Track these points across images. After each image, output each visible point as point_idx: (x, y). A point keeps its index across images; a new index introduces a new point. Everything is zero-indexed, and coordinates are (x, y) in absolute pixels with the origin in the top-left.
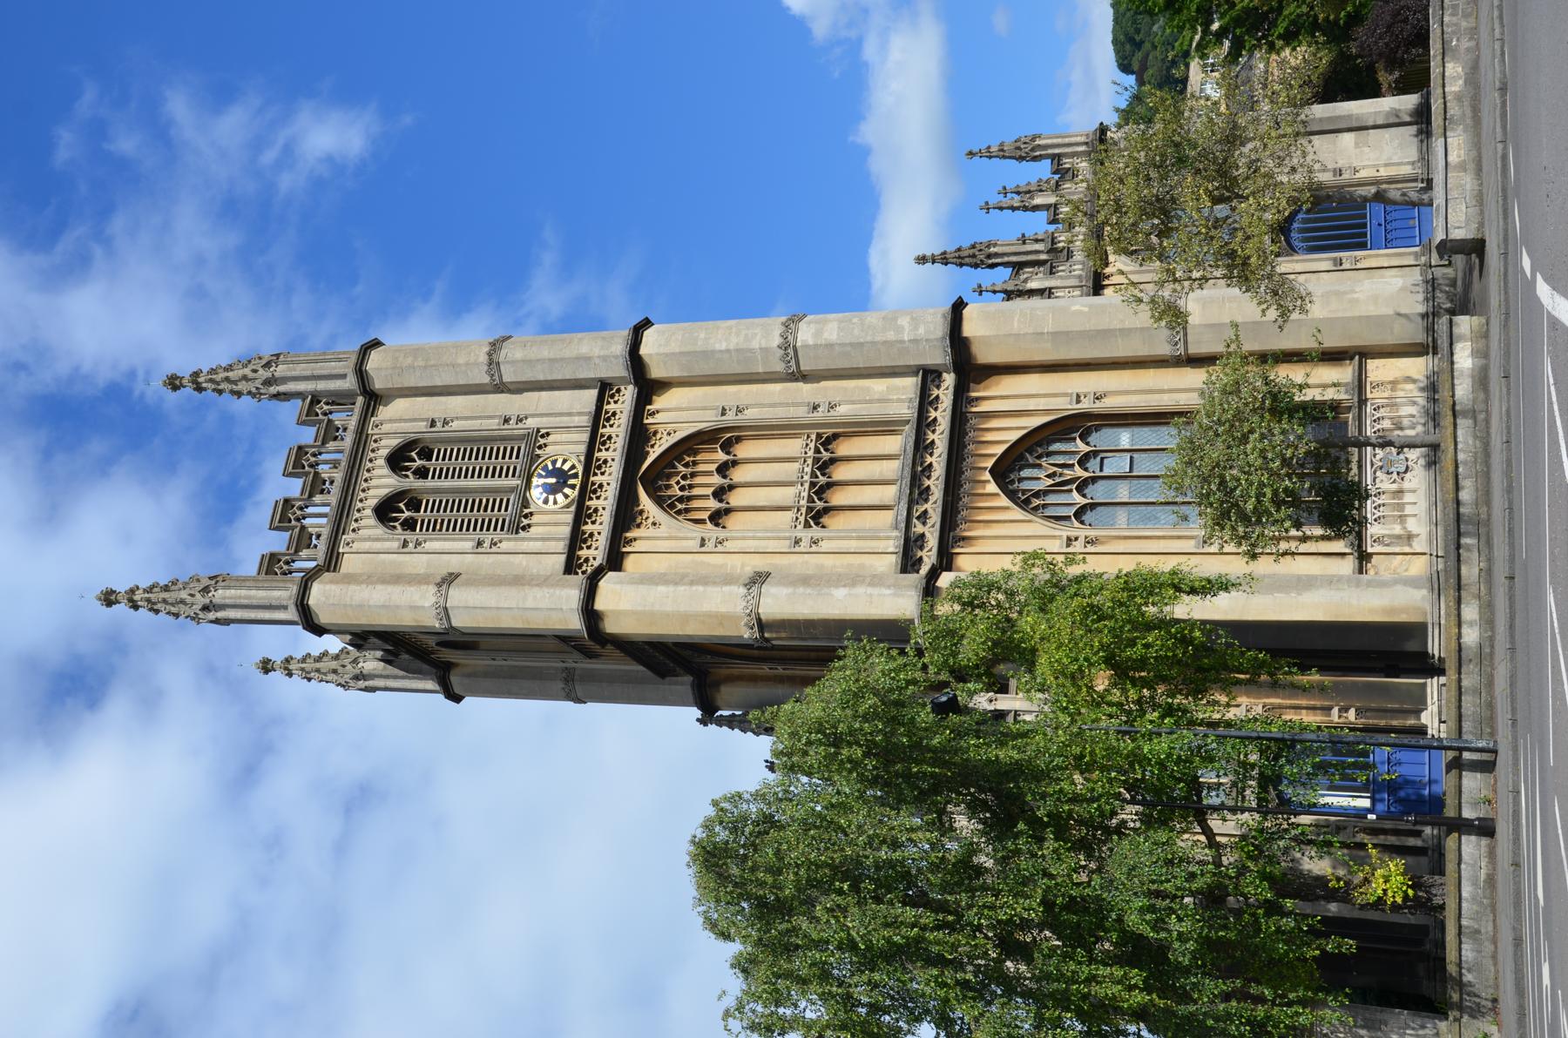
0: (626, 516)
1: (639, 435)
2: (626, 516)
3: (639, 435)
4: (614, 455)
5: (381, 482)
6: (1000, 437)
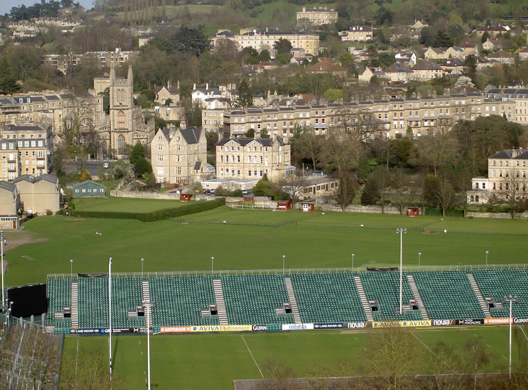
0: (118, 110)
1: (124, 109)
2: (118, 110)
3: (124, 109)
4: (123, 108)
5: (121, 89)
6: (123, 134)
